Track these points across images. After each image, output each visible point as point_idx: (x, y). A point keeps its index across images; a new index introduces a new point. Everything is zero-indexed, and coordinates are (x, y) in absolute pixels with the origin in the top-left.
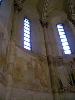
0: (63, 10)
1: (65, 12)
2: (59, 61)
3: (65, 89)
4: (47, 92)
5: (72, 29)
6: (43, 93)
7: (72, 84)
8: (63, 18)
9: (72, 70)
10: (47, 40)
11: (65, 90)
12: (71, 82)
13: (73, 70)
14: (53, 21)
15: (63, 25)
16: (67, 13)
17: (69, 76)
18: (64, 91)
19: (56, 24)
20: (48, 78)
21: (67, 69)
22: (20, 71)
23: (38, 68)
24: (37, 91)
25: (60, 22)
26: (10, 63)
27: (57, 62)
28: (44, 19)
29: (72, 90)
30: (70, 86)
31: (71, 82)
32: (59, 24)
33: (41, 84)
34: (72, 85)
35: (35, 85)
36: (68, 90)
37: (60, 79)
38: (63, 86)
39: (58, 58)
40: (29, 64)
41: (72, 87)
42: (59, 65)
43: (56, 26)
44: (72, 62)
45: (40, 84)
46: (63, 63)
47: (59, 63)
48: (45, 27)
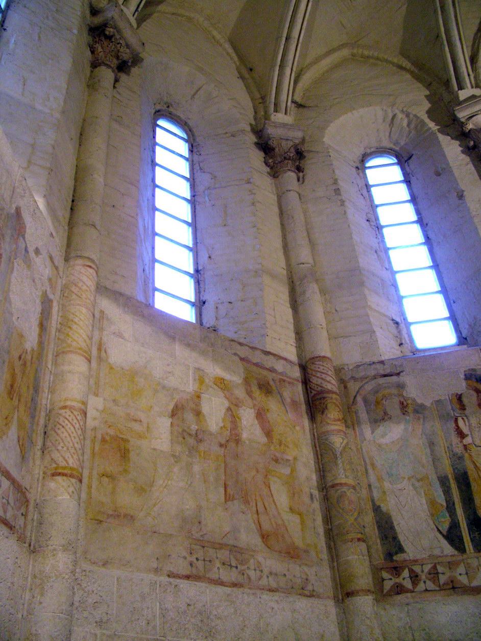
3: (417, 569)
6: (276, 596)
7: (461, 539)
8: (400, 116)
9: (459, 450)
11: (415, 578)
12: (454, 525)
13: (465, 446)
14: (342, 132)
15: (403, 160)
16: (428, 86)
18: (408, 584)
19: (361, 151)
20: (307, 500)
21: (432, 444)
22: (124, 454)
23: (245, 435)
24: (235, 585)
25: (386, 143)
26: (65, 407)
27: (365, 401)
28: (283, 124)
29: (464, 580)
30: (448, 549)
31: (454, 525)
32: (381, 151)
33: (265, 537)
34: (461, 548)
35: (222, 546)
36: (434, 574)
37: (384, 509)
38: (401, 549)
40: (184, 410)
42: (380, 418)
44: (459, 398)
45: (257, 541)
46: (403, 406)
47: (378, 403)
48: (290, 176)
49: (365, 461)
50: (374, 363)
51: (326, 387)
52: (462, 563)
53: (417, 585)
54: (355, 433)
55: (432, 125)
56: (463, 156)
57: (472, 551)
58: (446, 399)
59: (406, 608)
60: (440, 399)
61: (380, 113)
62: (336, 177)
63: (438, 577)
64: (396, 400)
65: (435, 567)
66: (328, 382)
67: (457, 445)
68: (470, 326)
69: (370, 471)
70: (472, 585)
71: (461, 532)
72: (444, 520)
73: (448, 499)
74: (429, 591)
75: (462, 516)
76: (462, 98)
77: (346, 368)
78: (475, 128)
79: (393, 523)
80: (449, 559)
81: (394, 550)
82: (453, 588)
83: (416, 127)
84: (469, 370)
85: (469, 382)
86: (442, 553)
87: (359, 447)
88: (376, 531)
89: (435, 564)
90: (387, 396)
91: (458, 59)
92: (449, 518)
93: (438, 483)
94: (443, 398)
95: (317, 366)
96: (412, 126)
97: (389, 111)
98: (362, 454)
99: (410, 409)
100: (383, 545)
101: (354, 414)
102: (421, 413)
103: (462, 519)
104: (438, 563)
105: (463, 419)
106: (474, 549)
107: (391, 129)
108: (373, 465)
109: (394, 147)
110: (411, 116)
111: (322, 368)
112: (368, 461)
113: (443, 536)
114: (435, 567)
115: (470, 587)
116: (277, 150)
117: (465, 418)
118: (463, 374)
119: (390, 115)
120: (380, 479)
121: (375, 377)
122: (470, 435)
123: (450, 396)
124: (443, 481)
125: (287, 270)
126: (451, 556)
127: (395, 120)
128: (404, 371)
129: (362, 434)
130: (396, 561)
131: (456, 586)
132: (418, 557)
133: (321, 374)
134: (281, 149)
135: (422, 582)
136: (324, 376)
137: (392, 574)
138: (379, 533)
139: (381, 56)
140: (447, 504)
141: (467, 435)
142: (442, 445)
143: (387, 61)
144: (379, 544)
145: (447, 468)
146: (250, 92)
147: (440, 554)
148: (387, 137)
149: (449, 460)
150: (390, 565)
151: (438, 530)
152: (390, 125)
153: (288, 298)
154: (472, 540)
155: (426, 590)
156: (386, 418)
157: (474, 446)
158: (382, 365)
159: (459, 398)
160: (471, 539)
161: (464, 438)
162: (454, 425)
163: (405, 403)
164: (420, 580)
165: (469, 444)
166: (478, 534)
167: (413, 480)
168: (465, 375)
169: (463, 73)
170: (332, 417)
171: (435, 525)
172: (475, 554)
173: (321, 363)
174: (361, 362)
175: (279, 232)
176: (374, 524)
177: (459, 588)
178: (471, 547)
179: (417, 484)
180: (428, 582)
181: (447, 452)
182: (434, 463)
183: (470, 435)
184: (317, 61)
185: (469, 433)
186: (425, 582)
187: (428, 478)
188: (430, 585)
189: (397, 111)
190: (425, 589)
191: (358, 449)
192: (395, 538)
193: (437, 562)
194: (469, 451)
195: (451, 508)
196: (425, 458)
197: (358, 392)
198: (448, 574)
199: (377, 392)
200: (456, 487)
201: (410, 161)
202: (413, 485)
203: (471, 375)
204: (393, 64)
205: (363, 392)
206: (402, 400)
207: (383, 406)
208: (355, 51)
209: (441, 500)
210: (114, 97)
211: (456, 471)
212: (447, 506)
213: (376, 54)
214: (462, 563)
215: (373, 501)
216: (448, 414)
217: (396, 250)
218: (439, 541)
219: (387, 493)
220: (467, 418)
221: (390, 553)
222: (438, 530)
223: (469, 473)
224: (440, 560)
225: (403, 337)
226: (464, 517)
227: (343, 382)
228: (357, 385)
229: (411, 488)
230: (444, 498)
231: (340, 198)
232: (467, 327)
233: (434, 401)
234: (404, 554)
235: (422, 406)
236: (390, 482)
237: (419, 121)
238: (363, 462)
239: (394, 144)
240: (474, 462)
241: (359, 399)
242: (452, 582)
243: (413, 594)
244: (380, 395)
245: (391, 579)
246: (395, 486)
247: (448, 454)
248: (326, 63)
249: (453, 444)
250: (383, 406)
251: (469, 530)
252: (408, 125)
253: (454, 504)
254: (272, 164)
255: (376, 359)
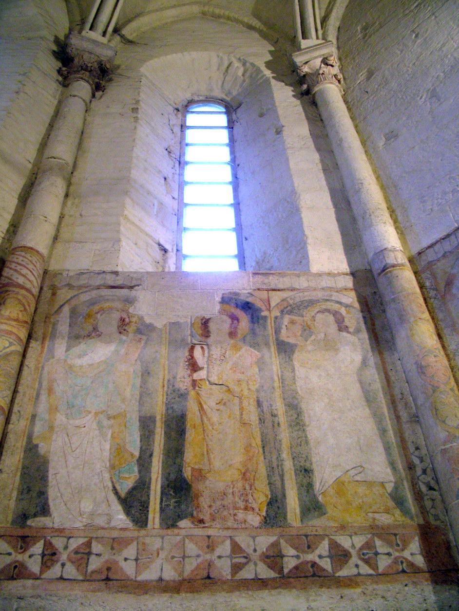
0: (256, 23)
1: (264, 36)
2: (92, 302)
3: (58, 543)
5: (283, 122)
7: (145, 507)
8: (236, 64)
9: (183, 384)
10: (62, 149)
12: (142, 485)
13: (194, 383)
14: (164, 72)
15: (231, 109)
16: (275, 43)
17: (137, 437)
18: (34, 566)
19: (188, 96)
21: (146, 373)
25: (218, 93)
27: (74, 312)
28: (93, 43)
29: (129, 569)
30: (120, 518)
31: (142, 485)
32: (209, 100)
34: (141, 521)
36: (84, 554)
37: (42, 450)
38: (45, 510)
39: (98, 281)
41: (133, 531)
43: (185, 108)
44: (205, 323)
46: (123, 325)
47: (89, 316)
49: (40, 384)
50: (104, 272)
51: (15, 280)
52: (135, 543)
53: (49, 567)
54: (43, 347)
55: (268, 73)
56: (294, 99)
57: (157, 525)
58: (186, 322)
59: (16, 604)
60: (178, 322)
61: (215, 61)
62: (140, 99)
63: (88, 559)
64: (116, 316)
65: (88, 544)
66: (23, 275)
67: (183, 380)
68: (257, 263)
69: (43, 397)
70: (139, 579)
71: (148, 496)
72: (128, 476)
73: (144, 448)
74: (66, 579)
75: (158, 473)
76: (303, 47)
77: (65, 274)
78: (310, 72)
79: (48, 471)
80: (115, 534)
81: (33, 511)
82: (108, 579)
83: (251, 76)
84: (230, 293)
85: (225, 306)
86: (108, 523)
87: (40, 365)
88: (18, 478)
89: (92, 538)
90: (105, 310)
91: (306, 17)
92: (137, 474)
93: (138, 424)
94: (182, 321)
95: (16, 256)
96: (248, 74)
97: (225, 58)
98: (41, 374)
99: (131, 329)
100: (19, 500)
101: (51, 326)
102: (145, 335)
103: (157, 478)
104: (97, 538)
105: (202, 348)
106: (161, 524)
107: (225, 78)
108: (50, 391)
109: (225, 97)
110: (248, 64)
111: (21, 258)
112: (45, 384)
113: (119, 498)
114: (88, 544)
115: (136, 581)
116: (76, 60)
117: (205, 347)
118: (221, 296)
119: (226, 64)
120: (53, 410)
121: (98, 288)
122: (206, 369)
123: (193, 319)
124: (146, 424)
125: (35, 165)
126: (121, 529)
127: (230, 68)
128: (141, 285)
129: (51, 352)
130: (30, 527)
131: (111, 576)
132: (67, 525)
133: (16, 265)
134: (82, 61)
135: (59, 564)
136: (19, 268)
137: (15, 547)
138: (21, 483)
139: (232, 15)
140: (140, 454)
141: (202, 368)
142: (161, 377)
143: (237, 21)
144: (14, 498)
145: (158, 408)
146: (69, 12)
147: (102, 524)
148: (219, 87)
149: (165, 397)
150: (20, 532)
151: (114, 488)
152: (224, 74)
153: (20, 190)
154: (162, 510)
155: (61, 578)
156: (93, 334)
157: (207, 382)
158: (114, 276)
159: (205, 323)
160: (161, 508)
161: (195, 371)
162: (187, 354)
163: (127, 320)
164: (57, 561)
165: (201, 380)
166: (176, 502)
167: (101, 416)
168: (223, 298)
169: (310, 24)
170: (7, 313)
171: (112, 482)
172: (161, 531)
173: (23, 254)
174: (88, 270)
175: (43, 130)
176: (17, 469)
177: (117, 580)
178: (157, 521)
179: (106, 422)
180: (69, 565)
181: (166, 386)
182: (141, 398)
183: (206, 369)
185: (206, 366)
186: (63, 565)
187: (125, 416)
188: (71, 571)
189: (233, 59)
190: (59, 575)
191: (37, 368)
192: (42, 494)
193: (95, 536)
194: (197, 388)
195: (144, 461)
196: (130, 391)
197: (67, 301)
198: (106, 557)
199: (93, 304)
200: (163, 432)
201: (239, 110)
202: (99, 423)
203: (230, 299)
204: (242, 23)
205: (74, 302)
206: (125, 316)
207: (94, 321)
208: (206, 9)
209: (134, 447)
210: (271, 484)
211: (170, 411)
212: (140, 457)
213: (227, 13)
214: (135, 543)
215: (30, 437)
216: (183, 340)
217: (192, 185)
218: (109, 506)
219: (57, 429)
220: (208, 348)
221: (25, 515)
222: (114, 488)
223: (189, 416)
224: (101, 533)
225: (167, 266)
226: (160, 476)
228: (71, 293)
229: (95, 426)
230: (139, 446)
231: (135, 115)
232: (254, 264)
233: (170, 323)
234: (48, 518)
235: (151, 328)
236: (67, 414)
237: (255, 69)
238: (37, 384)
239: (226, 95)
240: (200, 404)
241: (66, 309)
242: (109, 569)
243: (39, 581)
244: (96, 308)
245: (10, 554)
246: (71, 422)
247: (166, 389)
249: (178, 377)
250: (94, 321)
251: (162, 493)
252: (243, 75)
253: (151, 455)
254: (66, 72)
255: (108, 269)
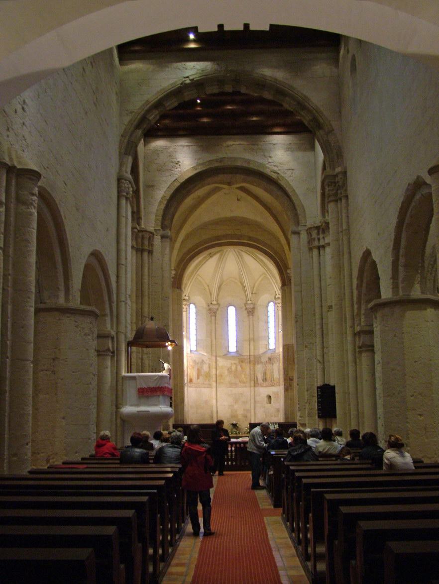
4: (246, 387)
30: (262, 382)
33: (240, 382)
42: (258, 364)
48: (251, 317)
184: (258, 279)
227: (255, 358)
248: (260, 279)
